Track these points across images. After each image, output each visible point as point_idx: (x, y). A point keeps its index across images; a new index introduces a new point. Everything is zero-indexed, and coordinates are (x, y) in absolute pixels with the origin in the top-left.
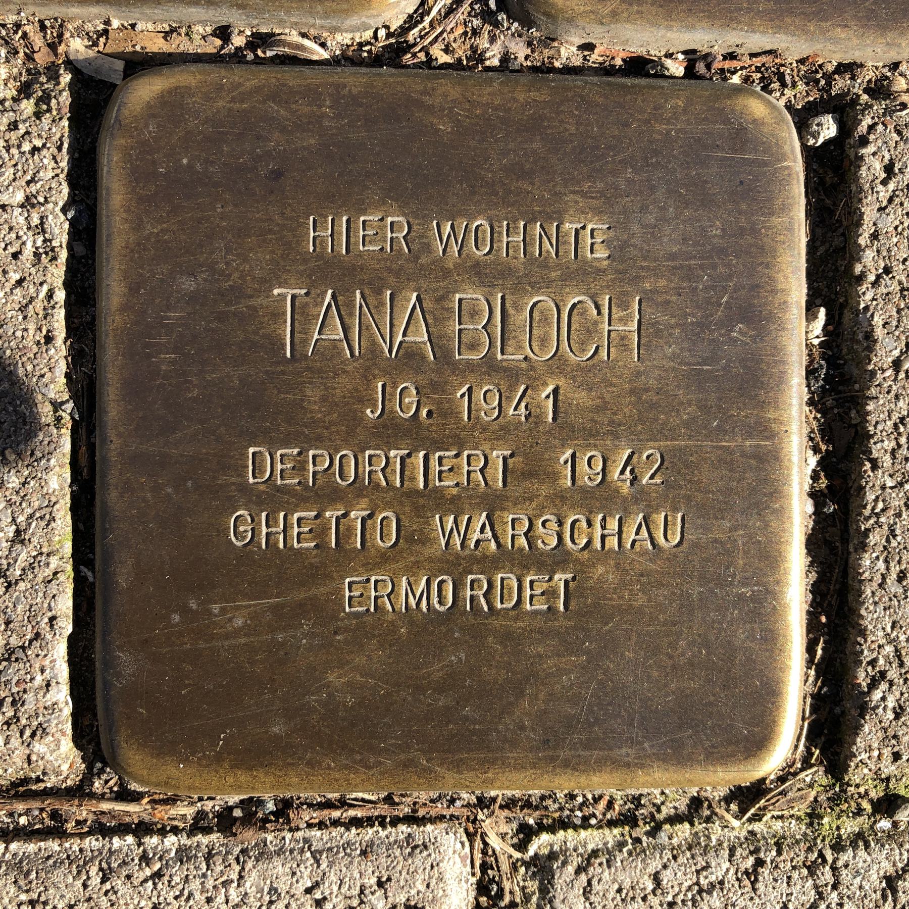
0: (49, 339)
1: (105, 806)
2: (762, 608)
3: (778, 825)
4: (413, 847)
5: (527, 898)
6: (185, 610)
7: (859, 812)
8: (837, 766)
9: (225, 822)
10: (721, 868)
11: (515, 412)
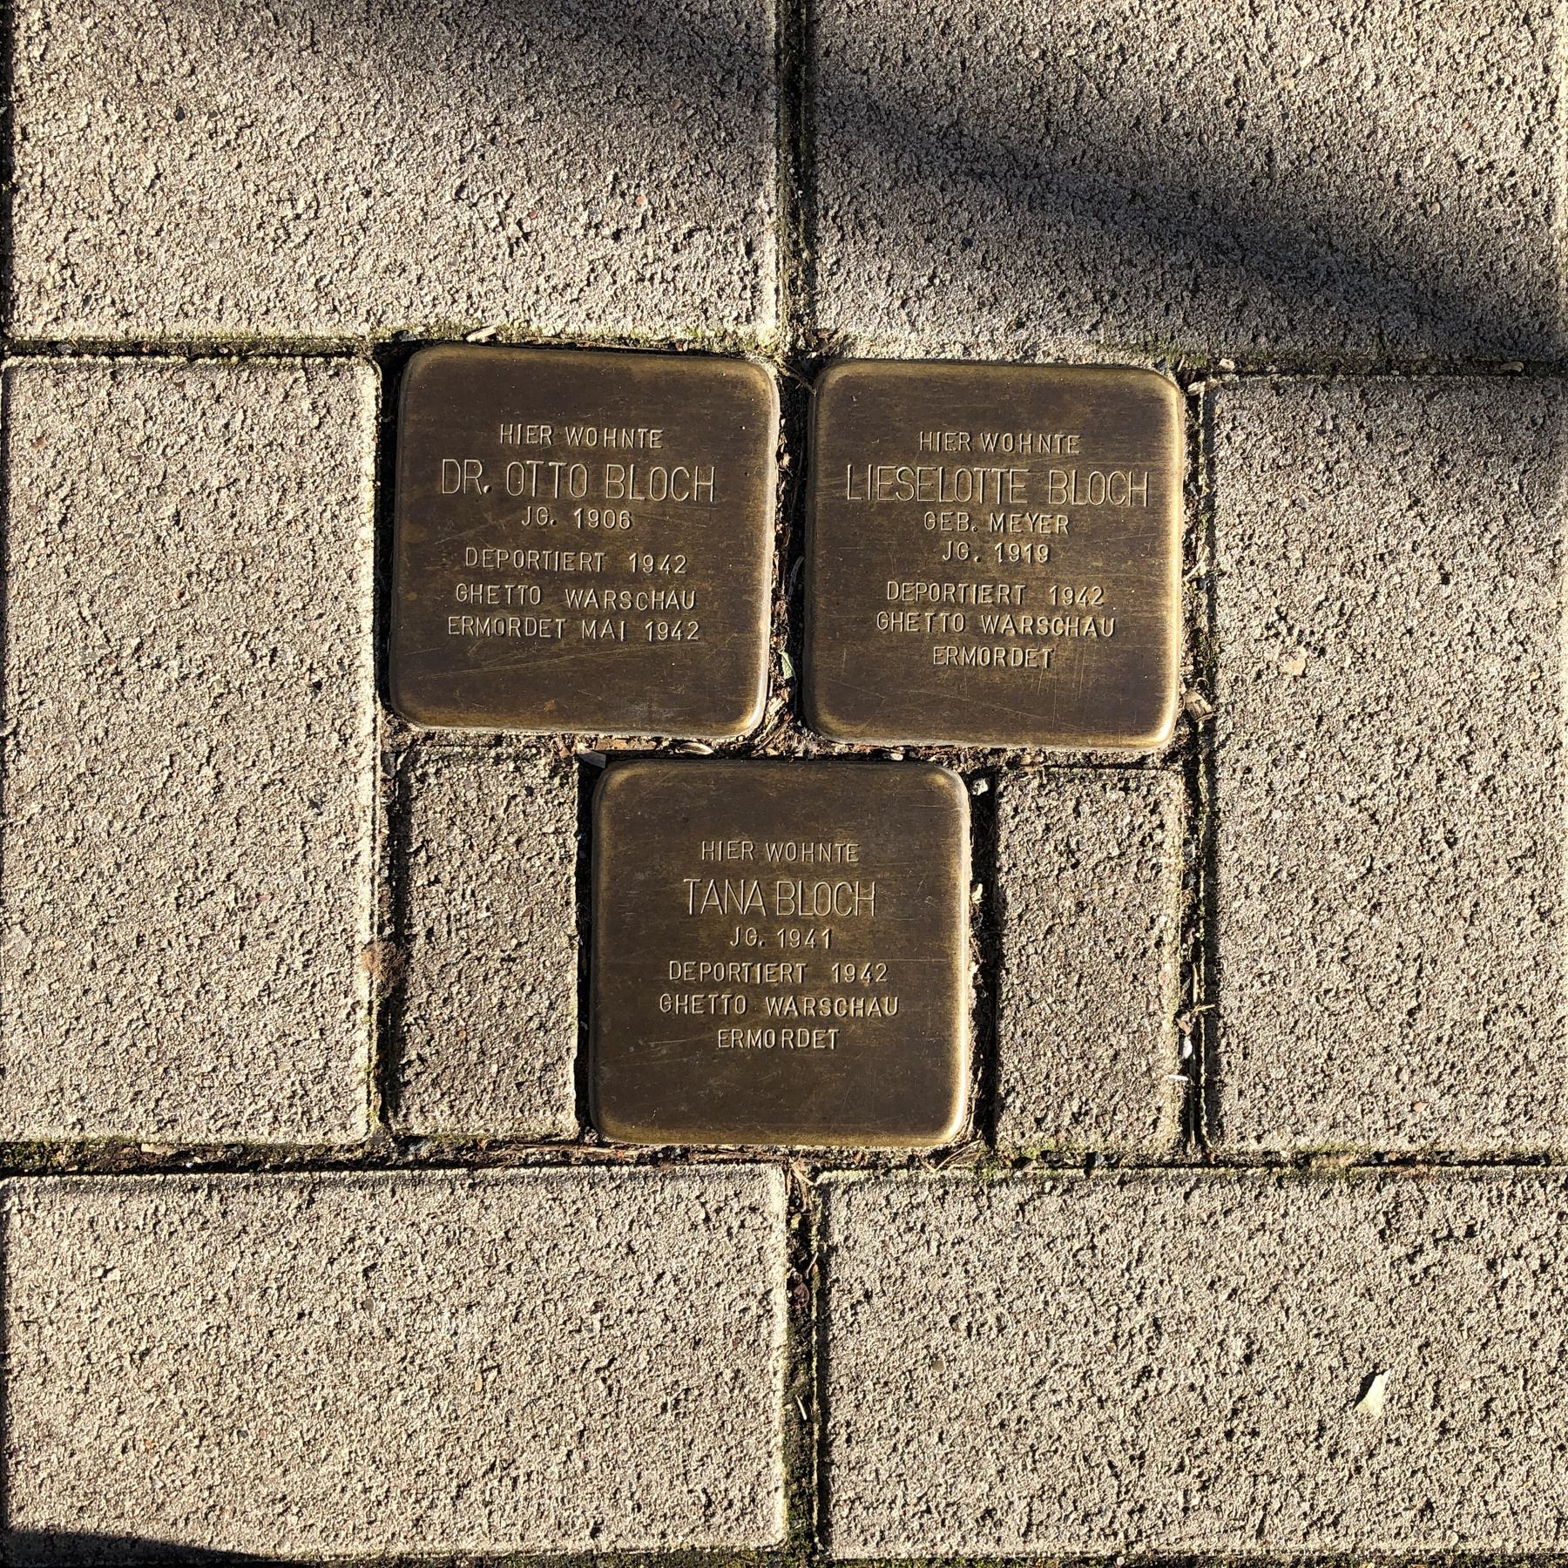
0: (568, 903)
1: (591, 1150)
2: (943, 1047)
3: (957, 1173)
4: (754, 1176)
5: (816, 1208)
6: (637, 1046)
7: (1005, 1166)
8: (991, 1140)
9: (654, 1160)
10: (924, 1194)
11: (809, 942)
